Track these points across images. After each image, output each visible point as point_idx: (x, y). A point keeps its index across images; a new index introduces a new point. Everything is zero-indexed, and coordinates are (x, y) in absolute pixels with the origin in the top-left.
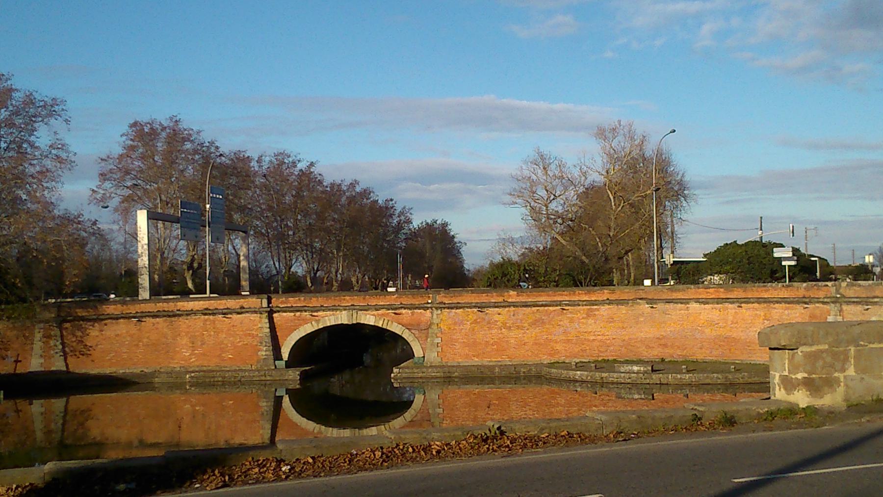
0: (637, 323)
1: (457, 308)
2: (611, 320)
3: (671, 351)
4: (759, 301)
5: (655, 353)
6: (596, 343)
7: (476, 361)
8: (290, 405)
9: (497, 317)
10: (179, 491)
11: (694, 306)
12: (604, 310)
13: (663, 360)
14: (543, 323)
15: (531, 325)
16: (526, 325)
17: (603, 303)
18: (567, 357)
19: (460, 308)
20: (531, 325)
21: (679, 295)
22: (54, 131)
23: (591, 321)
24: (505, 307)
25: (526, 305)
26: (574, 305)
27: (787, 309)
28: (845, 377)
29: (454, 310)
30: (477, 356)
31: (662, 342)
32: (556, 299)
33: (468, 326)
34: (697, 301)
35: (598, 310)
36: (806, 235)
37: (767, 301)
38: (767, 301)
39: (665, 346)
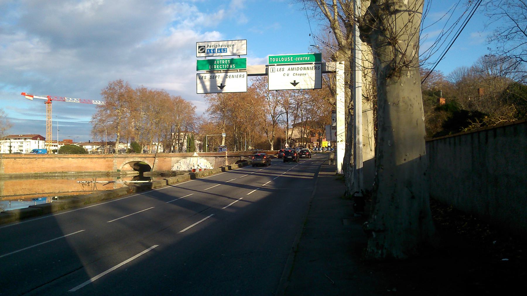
0: (55, 163)
1: (8, 158)
2: (49, 162)
3: (65, 170)
4: (89, 158)
5: (61, 170)
6: (45, 168)
7: (14, 173)
8: (151, 166)
9: (19, 161)
10: (216, 165)
11: (70, 159)
12: (47, 160)
13: (63, 172)
14: (31, 163)
15: (28, 163)
16: (27, 163)
17: (46, 158)
18: (38, 172)
19: (9, 158)
20: (28, 163)
21: (66, 156)
22: (406, 158)
23: (43, 162)
24: (21, 158)
25: (27, 158)
26: (39, 158)
27: (97, 159)
28: (496, 123)
29: (7, 159)
30: (15, 172)
31: (62, 167)
32: (34, 157)
33: (11, 163)
34: (72, 158)
35: (44, 160)
36: (39, 144)
37: (91, 158)
38: (91, 158)
39: (63, 168)
